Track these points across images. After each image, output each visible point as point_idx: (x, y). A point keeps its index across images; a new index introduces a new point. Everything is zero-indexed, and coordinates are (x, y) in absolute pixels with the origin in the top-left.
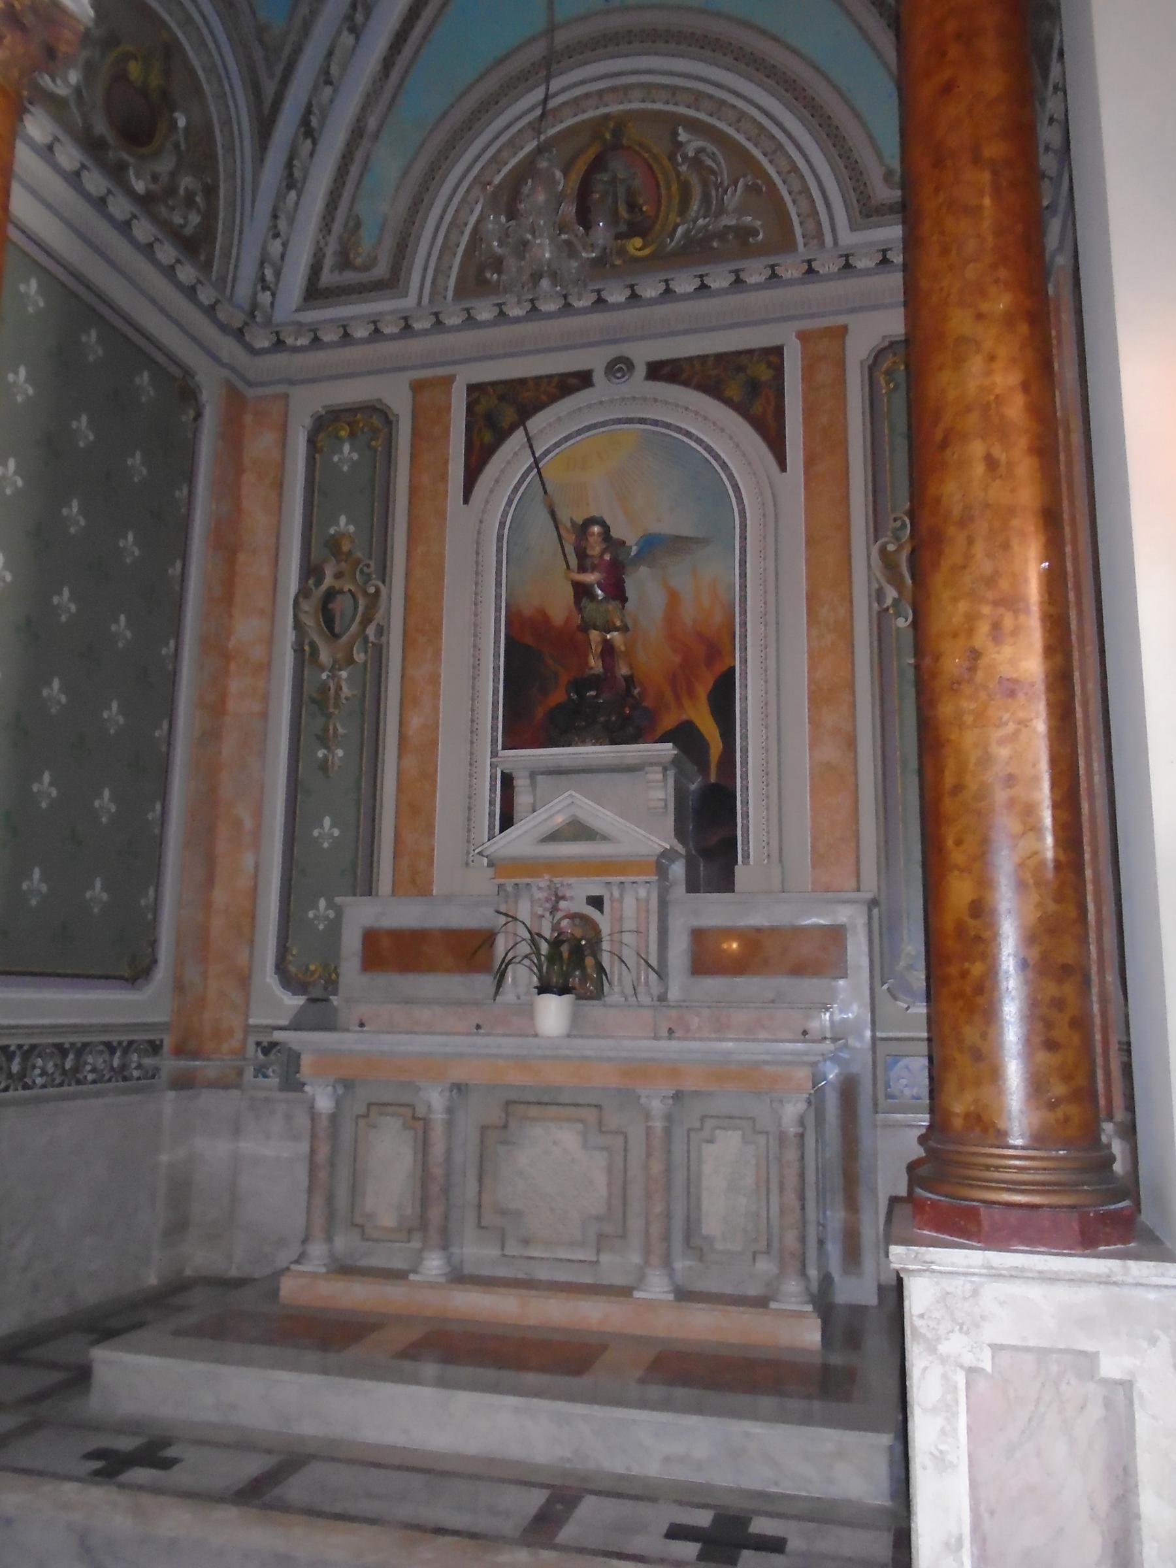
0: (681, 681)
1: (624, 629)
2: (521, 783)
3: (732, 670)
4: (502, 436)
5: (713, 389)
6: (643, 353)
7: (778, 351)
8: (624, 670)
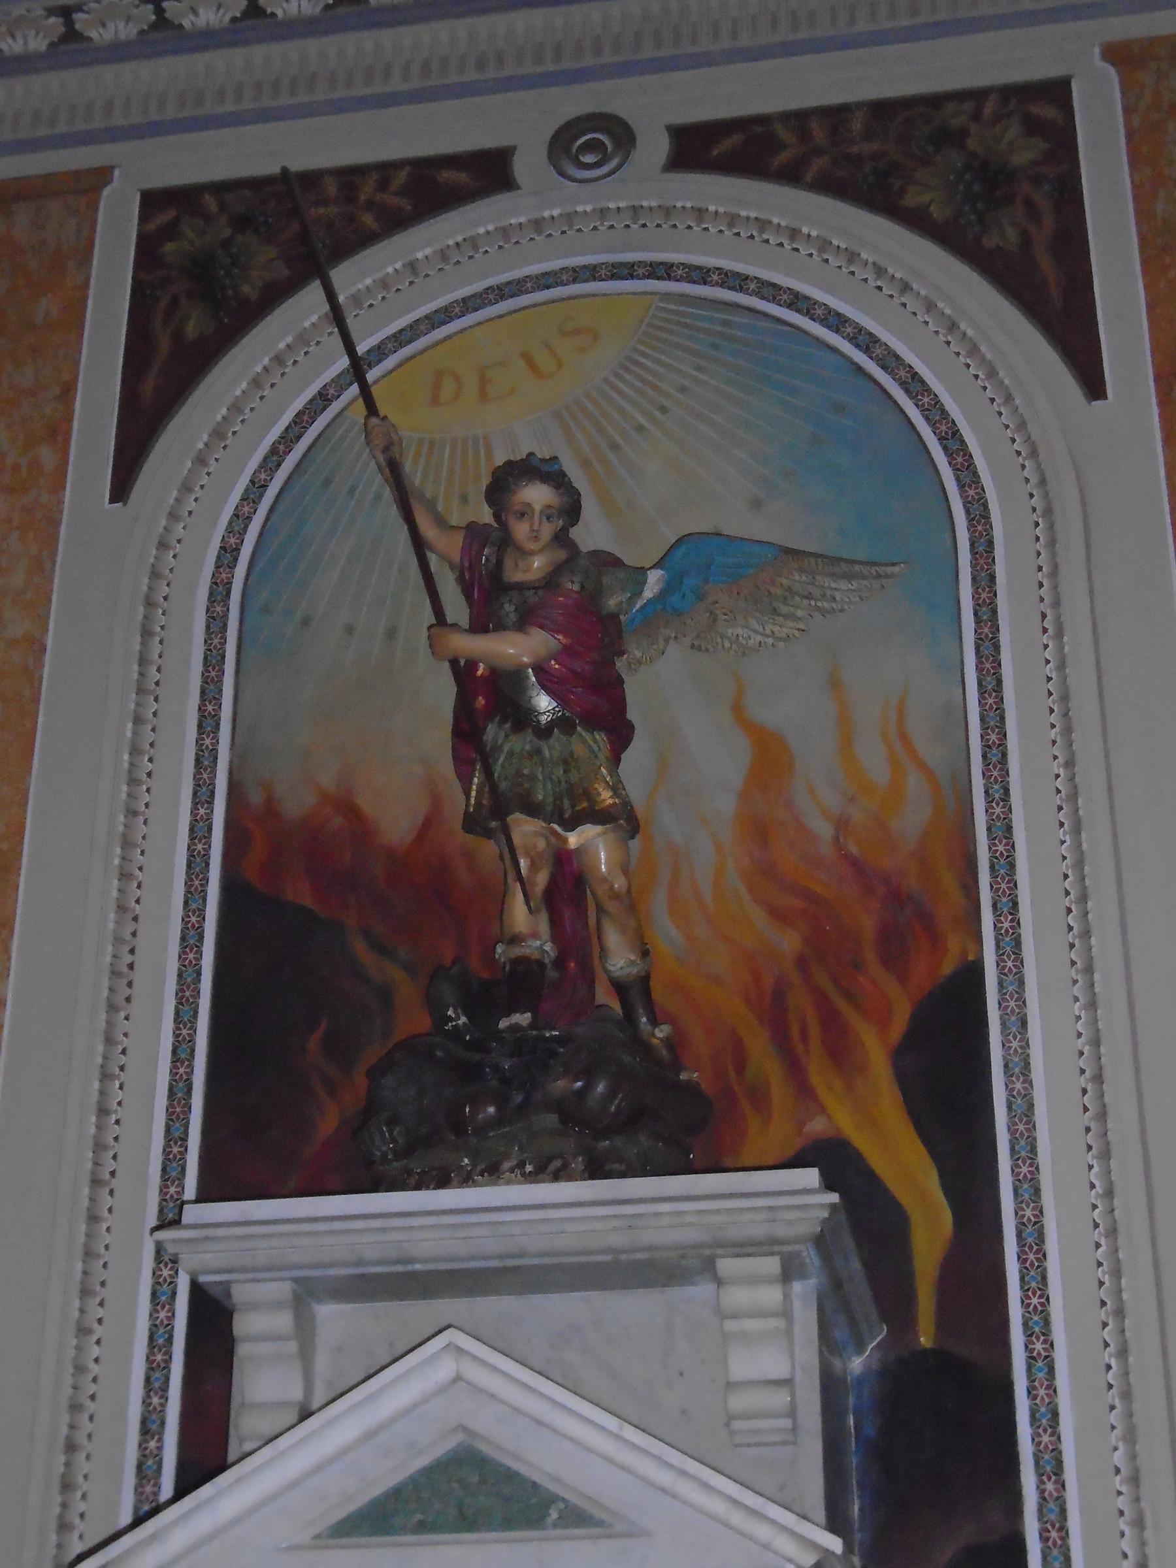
0: (801, 1013)
1: (625, 820)
2: (259, 1325)
3: (973, 973)
4: (238, 318)
5: (878, 192)
6: (657, 106)
7: (1057, 91)
8: (620, 959)
